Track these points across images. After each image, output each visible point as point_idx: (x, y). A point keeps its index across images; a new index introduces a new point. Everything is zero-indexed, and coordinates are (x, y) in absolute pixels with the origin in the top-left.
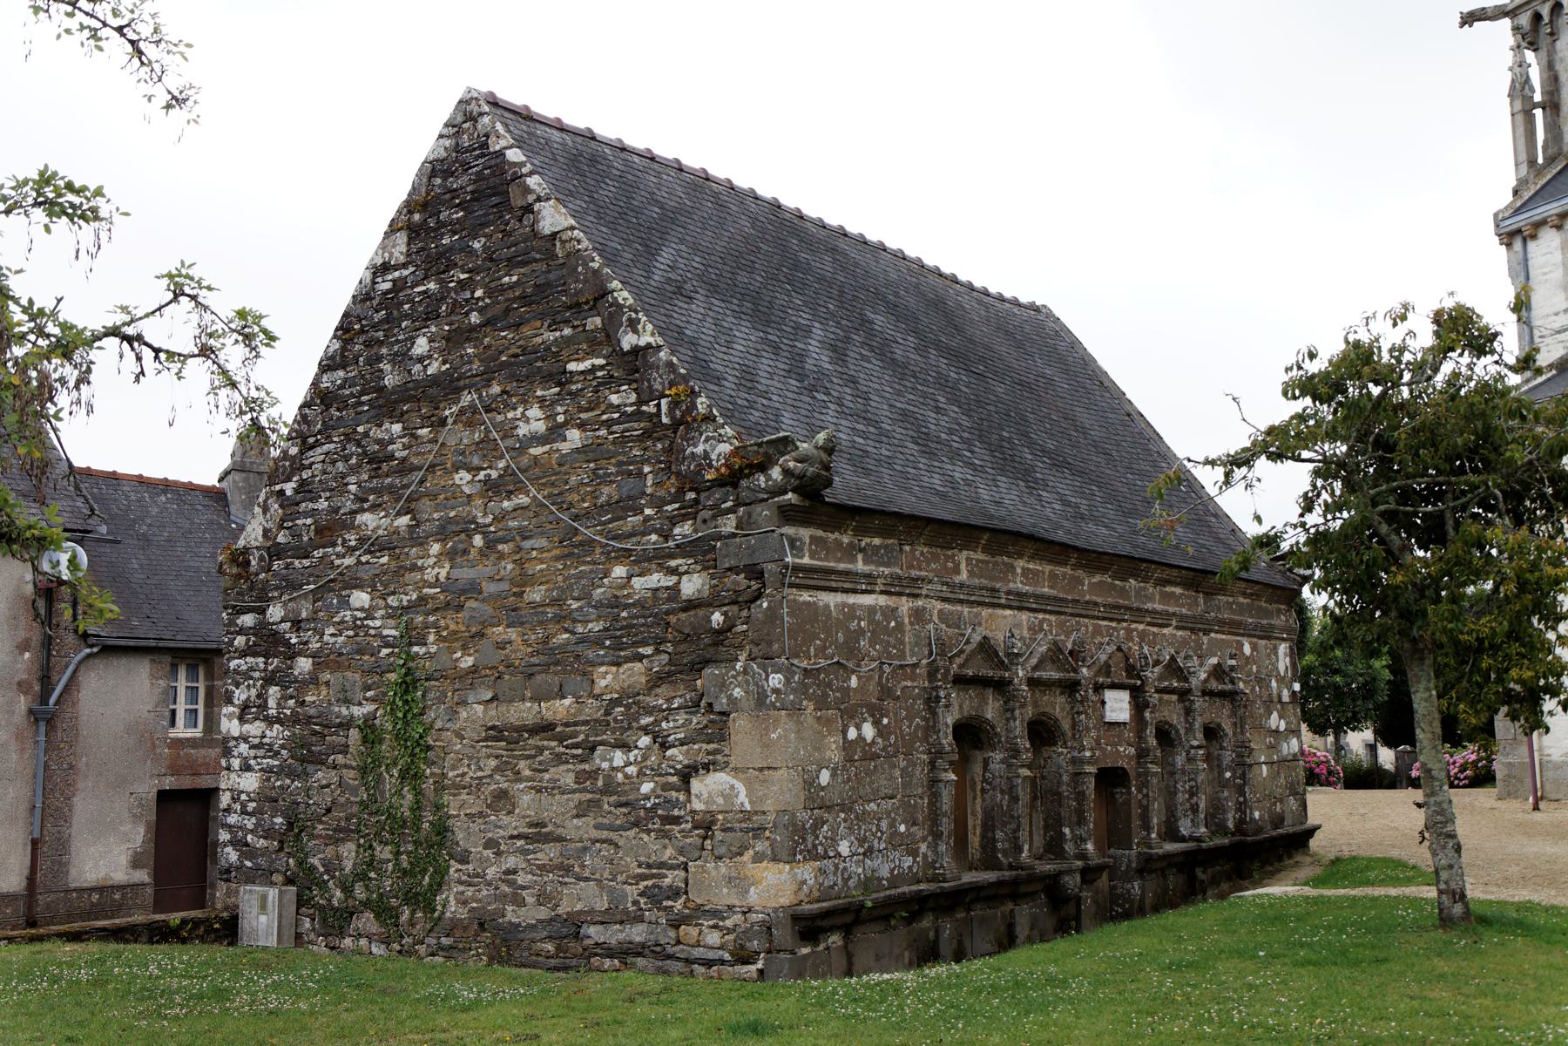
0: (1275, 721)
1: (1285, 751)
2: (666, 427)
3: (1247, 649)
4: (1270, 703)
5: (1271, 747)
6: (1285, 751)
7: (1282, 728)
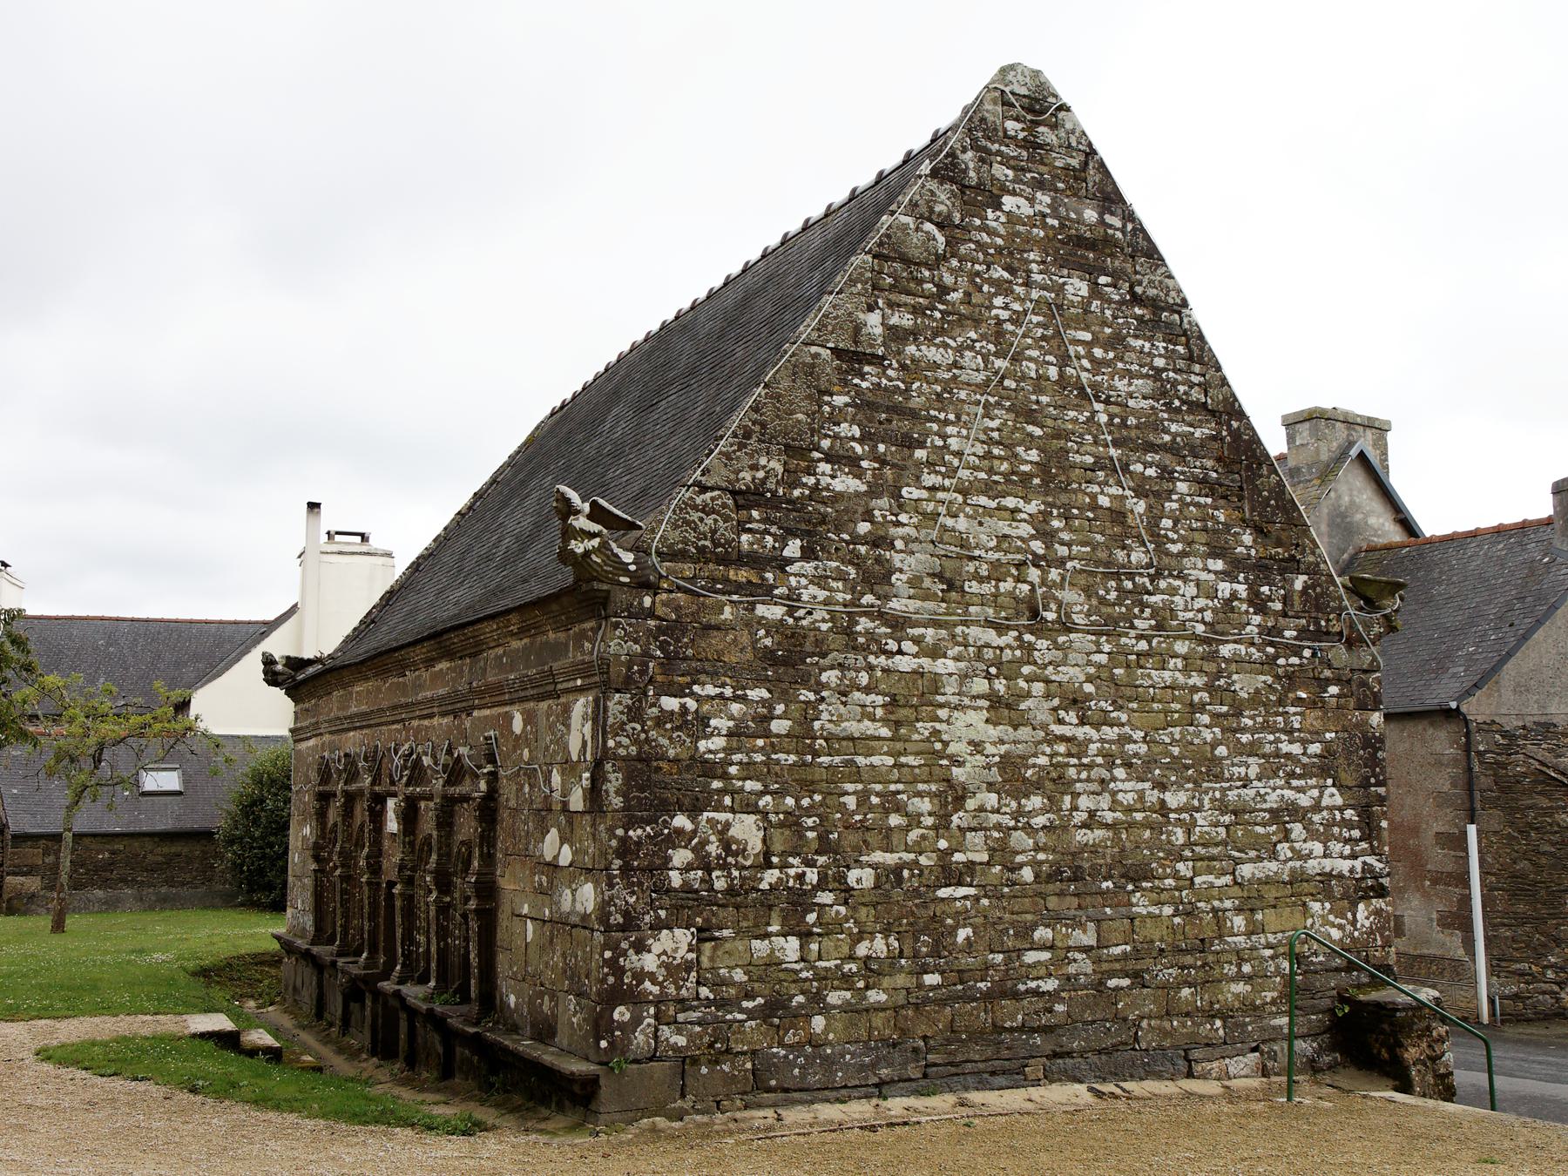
0: (552, 846)
1: (566, 906)
2: (664, 889)
3: (518, 725)
4: (544, 814)
5: (541, 891)
6: (566, 906)
7: (566, 857)
